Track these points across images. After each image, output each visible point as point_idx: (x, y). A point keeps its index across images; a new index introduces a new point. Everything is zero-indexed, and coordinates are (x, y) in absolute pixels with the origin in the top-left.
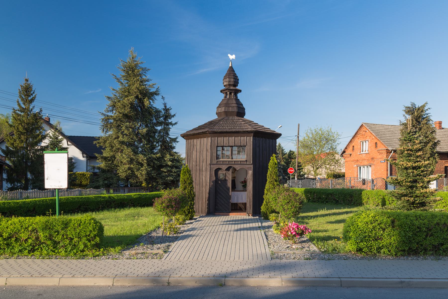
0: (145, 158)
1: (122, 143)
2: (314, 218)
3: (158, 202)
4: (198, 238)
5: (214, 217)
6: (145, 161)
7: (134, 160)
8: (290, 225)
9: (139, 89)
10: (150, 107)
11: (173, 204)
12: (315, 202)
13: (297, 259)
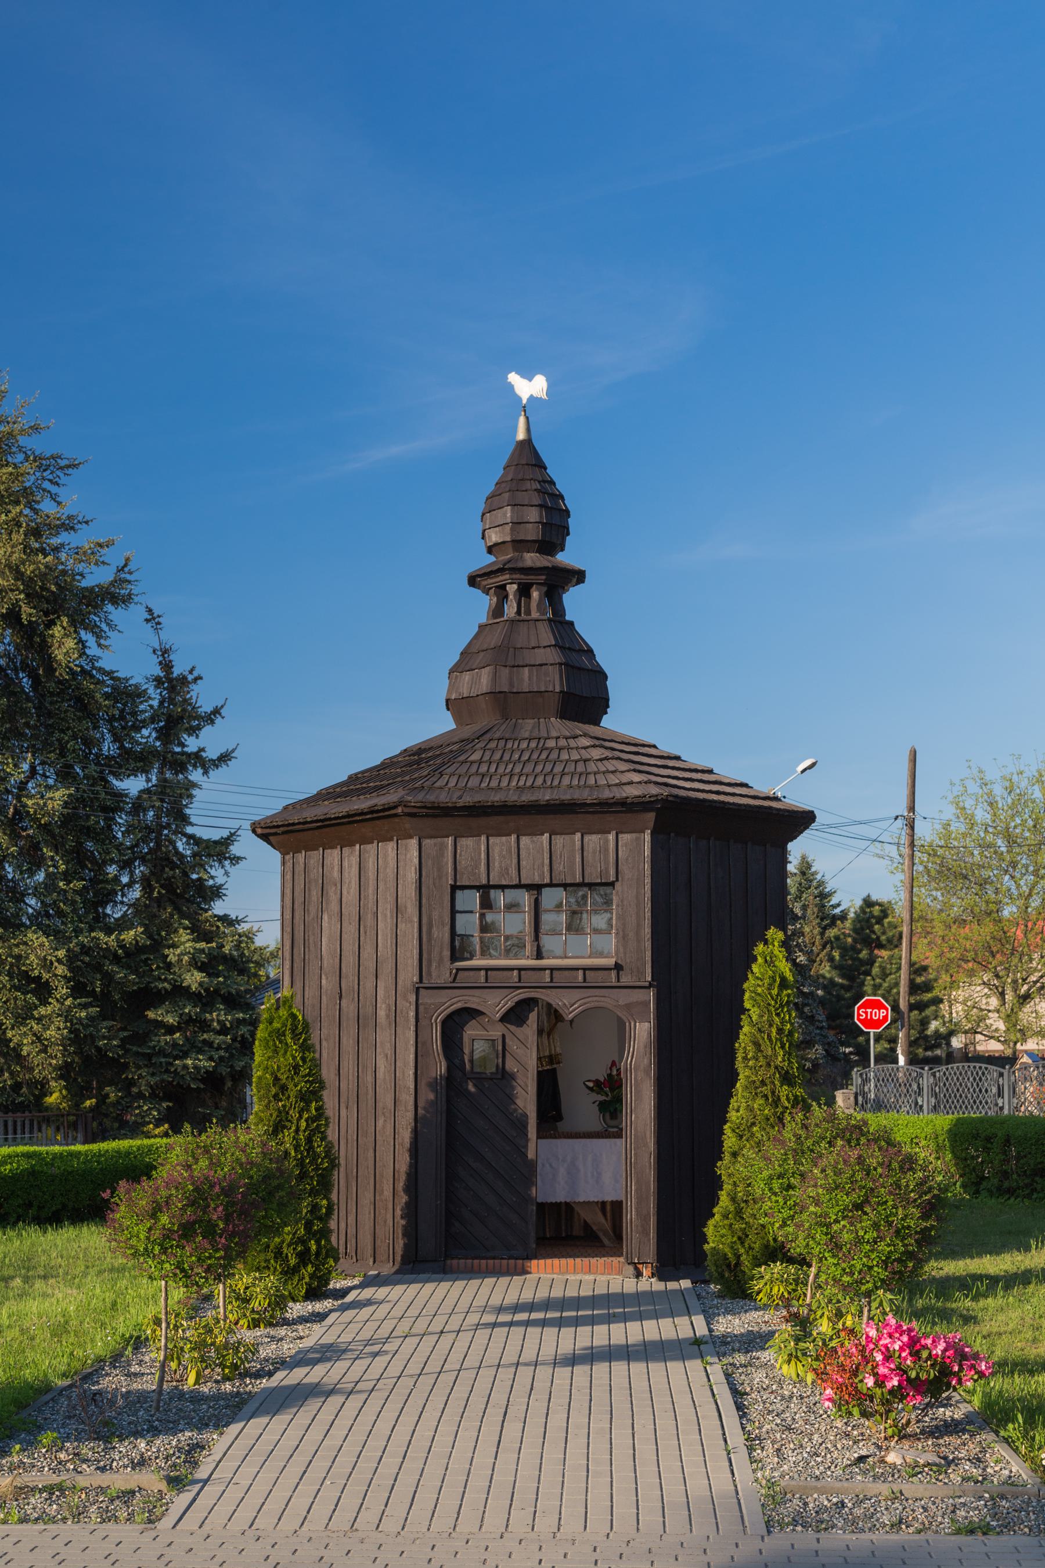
0: (61, 953)
2: (1007, 1288)
3: (131, 1203)
4: (354, 1402)
5: (445, 1285)
6: (61, 970)
8: (873, 1333)
9: (22, 574)
10: (84, 671)
11: (216, 1215)
12: (1011, 1192)
13: (911, 1530)
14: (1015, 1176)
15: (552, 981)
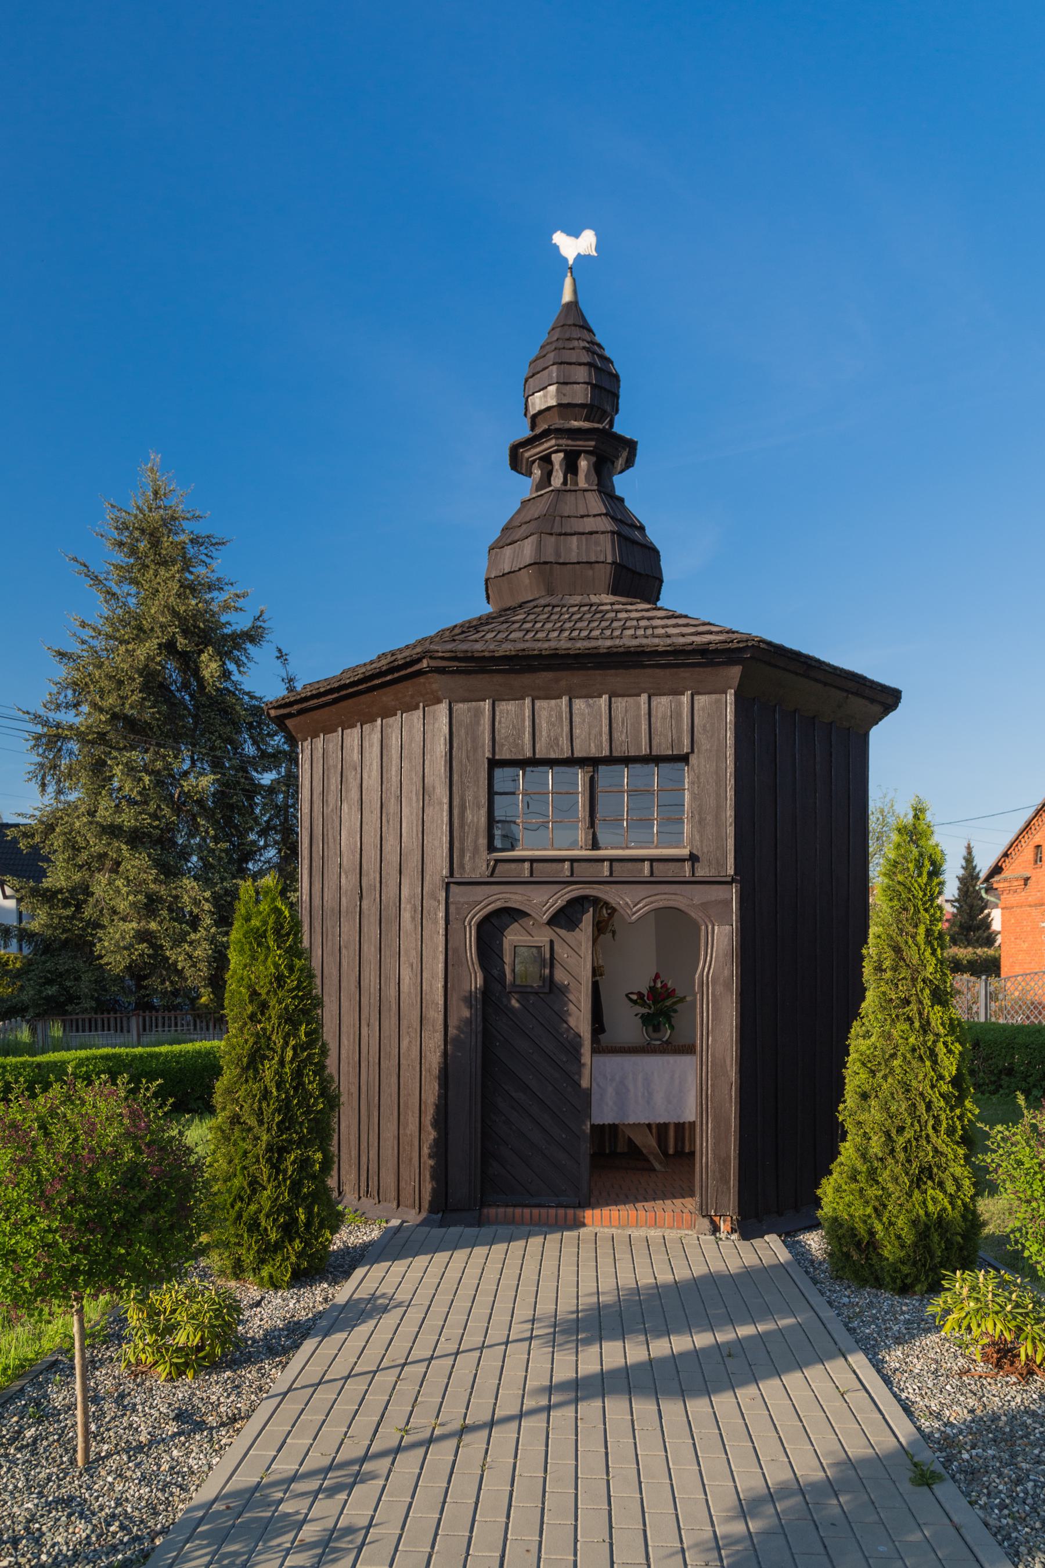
0: (207, 894)
1: (112, 831)
6: (207, 906)
7: (160, 900)
9: (178, 613)
14: (981, 1074)
15: (611, 875)
